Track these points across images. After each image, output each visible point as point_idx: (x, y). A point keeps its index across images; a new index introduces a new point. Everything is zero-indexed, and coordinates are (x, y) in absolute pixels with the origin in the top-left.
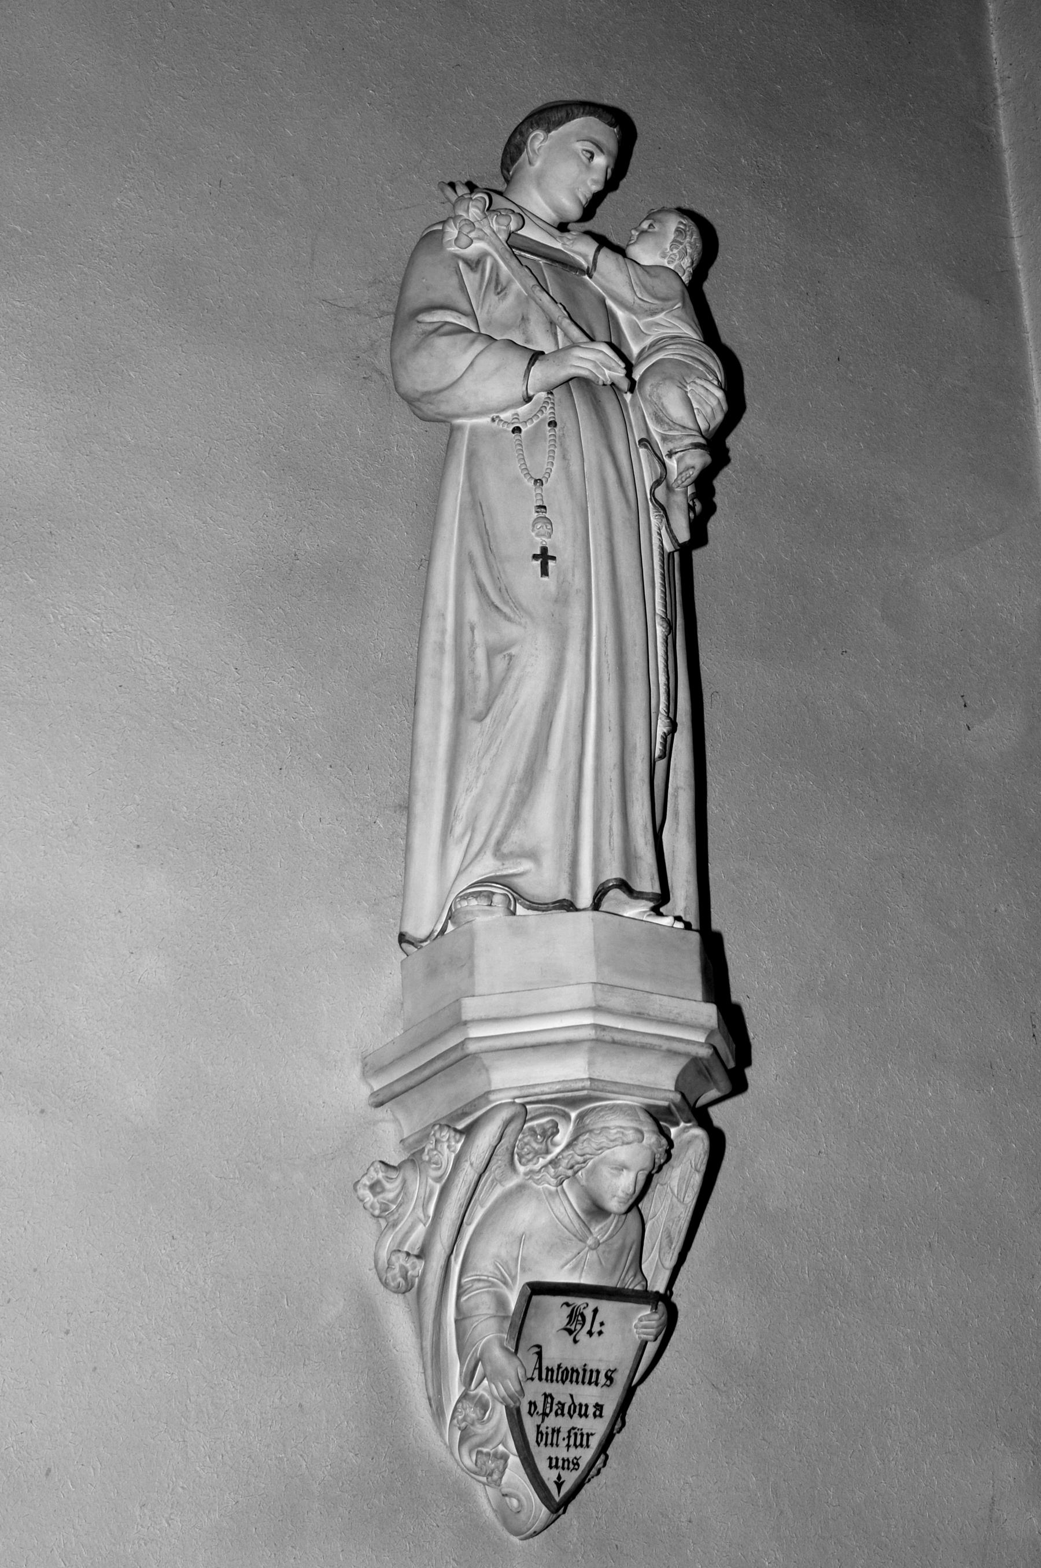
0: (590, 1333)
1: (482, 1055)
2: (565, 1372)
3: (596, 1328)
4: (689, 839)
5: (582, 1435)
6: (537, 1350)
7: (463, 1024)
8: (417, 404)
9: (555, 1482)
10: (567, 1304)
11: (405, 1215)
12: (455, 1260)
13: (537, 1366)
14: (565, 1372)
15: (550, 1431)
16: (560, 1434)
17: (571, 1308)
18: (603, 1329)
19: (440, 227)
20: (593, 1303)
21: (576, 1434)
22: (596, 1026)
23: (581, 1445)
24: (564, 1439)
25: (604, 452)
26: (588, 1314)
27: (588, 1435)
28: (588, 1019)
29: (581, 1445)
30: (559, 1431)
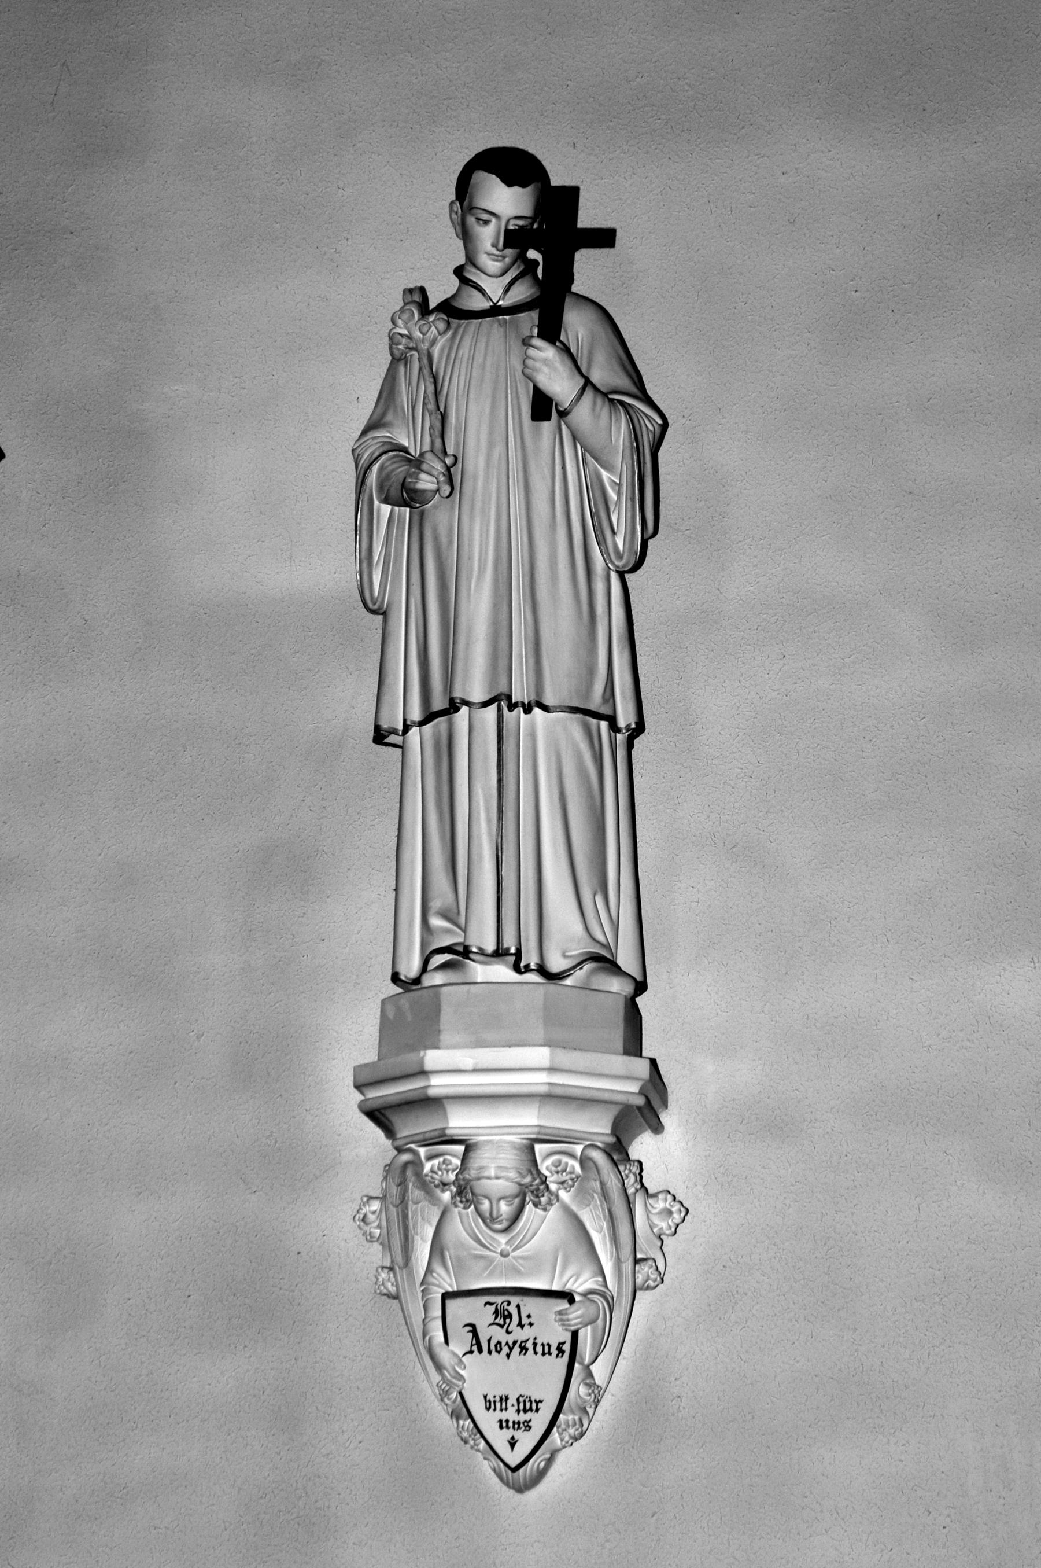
0: (521, 1325)
1: (445, 1101)
2: (498, 1346)
3: (525, 1321)
4: (452, 1220)
5: (530, 1401)
6: (470, 1328)
7: (423, 1073)
8: (415, 1193)
9: (509, 1442)
10: (491, 1304)
11: (514, 1264)
12: (377, 543)
13: (474, 1342)
14: (498, 1346)
15: (498, 1399)
16: (508, 1401)
17: (494, 1306)
18: (532, 1320)
19: (387, 734)
20: (515, 1300)
21: (525, 1401)
22: (550, 1084)
23: (531, 1409)
24: (513, 1405)
25: (557, 431)
26: (513, 1309)
27: (537, 1402)
28: (543, 1077)
29: (531, 1409)
30: (507, 1398)
